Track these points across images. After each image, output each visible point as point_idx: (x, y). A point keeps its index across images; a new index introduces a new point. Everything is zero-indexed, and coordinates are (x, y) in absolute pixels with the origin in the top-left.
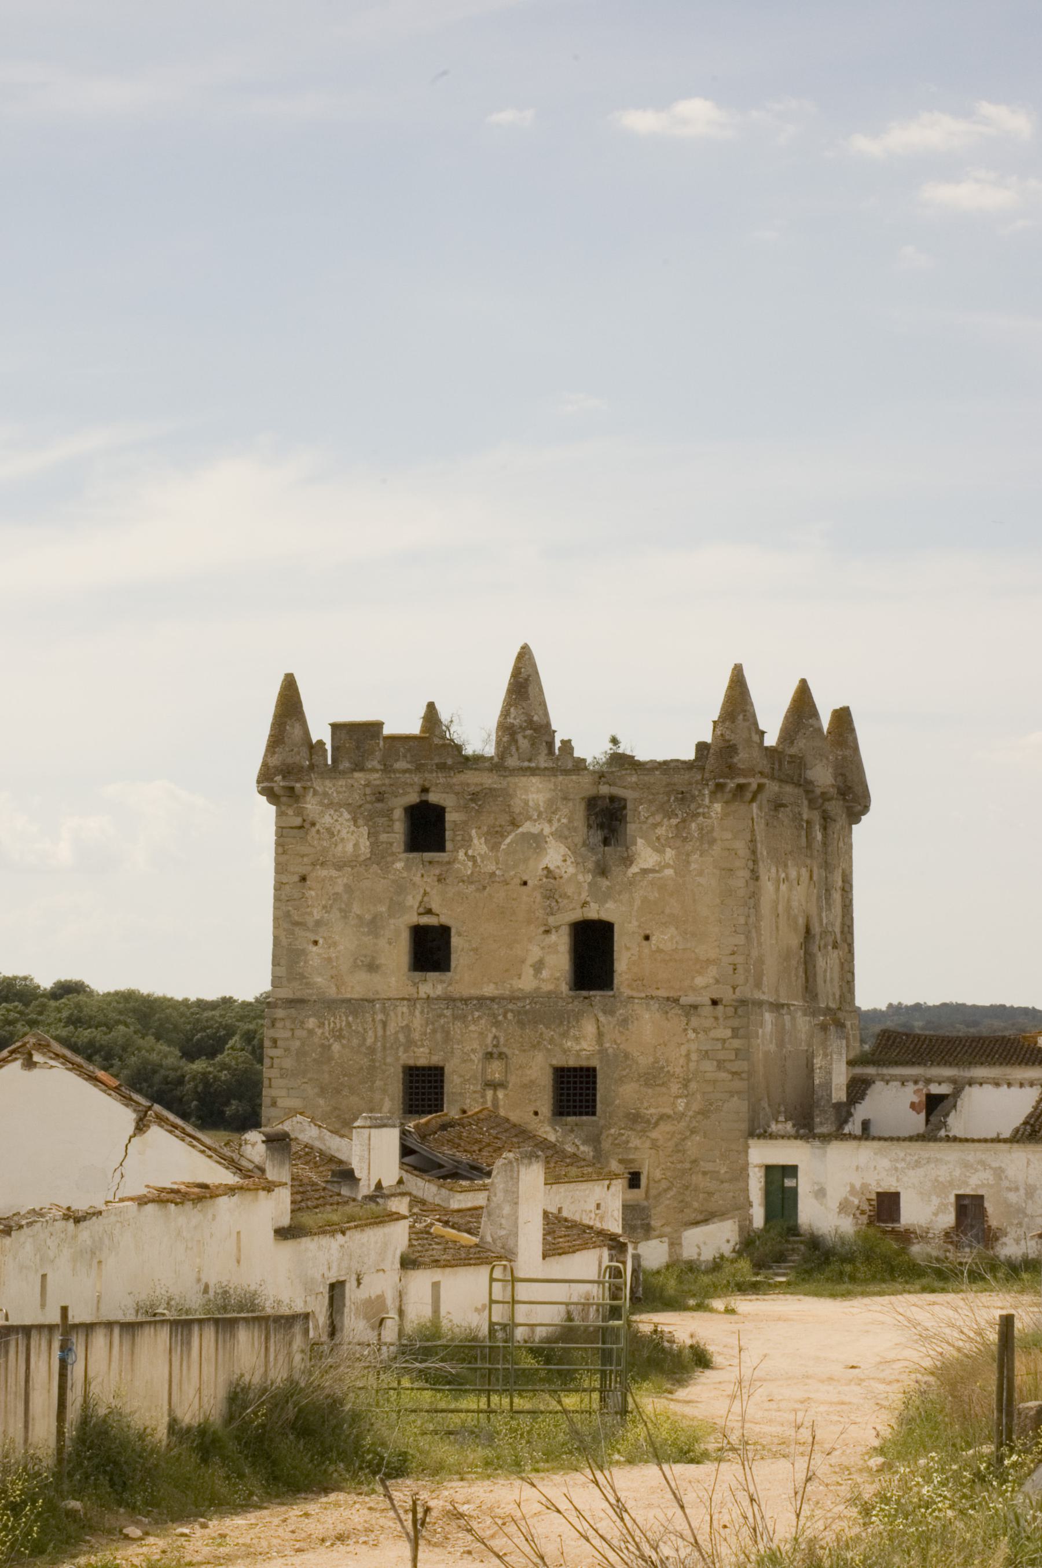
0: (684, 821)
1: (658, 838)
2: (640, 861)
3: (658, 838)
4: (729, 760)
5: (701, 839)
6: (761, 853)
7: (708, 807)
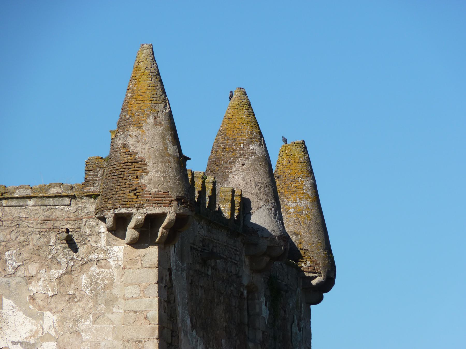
0: (69, 272)
1: (33, 298)
2: (8, 332)
3: (33, 298)
4: (135, 181)
5: (95, 297)
6: (183, 321)
7: (105, 251)
